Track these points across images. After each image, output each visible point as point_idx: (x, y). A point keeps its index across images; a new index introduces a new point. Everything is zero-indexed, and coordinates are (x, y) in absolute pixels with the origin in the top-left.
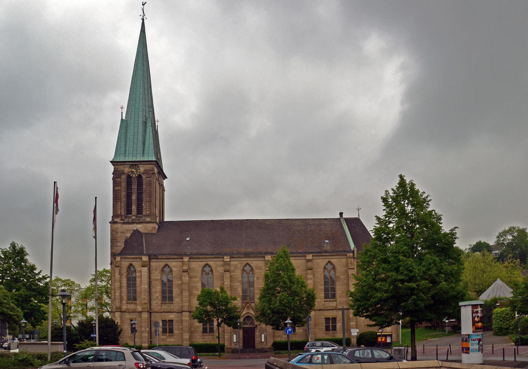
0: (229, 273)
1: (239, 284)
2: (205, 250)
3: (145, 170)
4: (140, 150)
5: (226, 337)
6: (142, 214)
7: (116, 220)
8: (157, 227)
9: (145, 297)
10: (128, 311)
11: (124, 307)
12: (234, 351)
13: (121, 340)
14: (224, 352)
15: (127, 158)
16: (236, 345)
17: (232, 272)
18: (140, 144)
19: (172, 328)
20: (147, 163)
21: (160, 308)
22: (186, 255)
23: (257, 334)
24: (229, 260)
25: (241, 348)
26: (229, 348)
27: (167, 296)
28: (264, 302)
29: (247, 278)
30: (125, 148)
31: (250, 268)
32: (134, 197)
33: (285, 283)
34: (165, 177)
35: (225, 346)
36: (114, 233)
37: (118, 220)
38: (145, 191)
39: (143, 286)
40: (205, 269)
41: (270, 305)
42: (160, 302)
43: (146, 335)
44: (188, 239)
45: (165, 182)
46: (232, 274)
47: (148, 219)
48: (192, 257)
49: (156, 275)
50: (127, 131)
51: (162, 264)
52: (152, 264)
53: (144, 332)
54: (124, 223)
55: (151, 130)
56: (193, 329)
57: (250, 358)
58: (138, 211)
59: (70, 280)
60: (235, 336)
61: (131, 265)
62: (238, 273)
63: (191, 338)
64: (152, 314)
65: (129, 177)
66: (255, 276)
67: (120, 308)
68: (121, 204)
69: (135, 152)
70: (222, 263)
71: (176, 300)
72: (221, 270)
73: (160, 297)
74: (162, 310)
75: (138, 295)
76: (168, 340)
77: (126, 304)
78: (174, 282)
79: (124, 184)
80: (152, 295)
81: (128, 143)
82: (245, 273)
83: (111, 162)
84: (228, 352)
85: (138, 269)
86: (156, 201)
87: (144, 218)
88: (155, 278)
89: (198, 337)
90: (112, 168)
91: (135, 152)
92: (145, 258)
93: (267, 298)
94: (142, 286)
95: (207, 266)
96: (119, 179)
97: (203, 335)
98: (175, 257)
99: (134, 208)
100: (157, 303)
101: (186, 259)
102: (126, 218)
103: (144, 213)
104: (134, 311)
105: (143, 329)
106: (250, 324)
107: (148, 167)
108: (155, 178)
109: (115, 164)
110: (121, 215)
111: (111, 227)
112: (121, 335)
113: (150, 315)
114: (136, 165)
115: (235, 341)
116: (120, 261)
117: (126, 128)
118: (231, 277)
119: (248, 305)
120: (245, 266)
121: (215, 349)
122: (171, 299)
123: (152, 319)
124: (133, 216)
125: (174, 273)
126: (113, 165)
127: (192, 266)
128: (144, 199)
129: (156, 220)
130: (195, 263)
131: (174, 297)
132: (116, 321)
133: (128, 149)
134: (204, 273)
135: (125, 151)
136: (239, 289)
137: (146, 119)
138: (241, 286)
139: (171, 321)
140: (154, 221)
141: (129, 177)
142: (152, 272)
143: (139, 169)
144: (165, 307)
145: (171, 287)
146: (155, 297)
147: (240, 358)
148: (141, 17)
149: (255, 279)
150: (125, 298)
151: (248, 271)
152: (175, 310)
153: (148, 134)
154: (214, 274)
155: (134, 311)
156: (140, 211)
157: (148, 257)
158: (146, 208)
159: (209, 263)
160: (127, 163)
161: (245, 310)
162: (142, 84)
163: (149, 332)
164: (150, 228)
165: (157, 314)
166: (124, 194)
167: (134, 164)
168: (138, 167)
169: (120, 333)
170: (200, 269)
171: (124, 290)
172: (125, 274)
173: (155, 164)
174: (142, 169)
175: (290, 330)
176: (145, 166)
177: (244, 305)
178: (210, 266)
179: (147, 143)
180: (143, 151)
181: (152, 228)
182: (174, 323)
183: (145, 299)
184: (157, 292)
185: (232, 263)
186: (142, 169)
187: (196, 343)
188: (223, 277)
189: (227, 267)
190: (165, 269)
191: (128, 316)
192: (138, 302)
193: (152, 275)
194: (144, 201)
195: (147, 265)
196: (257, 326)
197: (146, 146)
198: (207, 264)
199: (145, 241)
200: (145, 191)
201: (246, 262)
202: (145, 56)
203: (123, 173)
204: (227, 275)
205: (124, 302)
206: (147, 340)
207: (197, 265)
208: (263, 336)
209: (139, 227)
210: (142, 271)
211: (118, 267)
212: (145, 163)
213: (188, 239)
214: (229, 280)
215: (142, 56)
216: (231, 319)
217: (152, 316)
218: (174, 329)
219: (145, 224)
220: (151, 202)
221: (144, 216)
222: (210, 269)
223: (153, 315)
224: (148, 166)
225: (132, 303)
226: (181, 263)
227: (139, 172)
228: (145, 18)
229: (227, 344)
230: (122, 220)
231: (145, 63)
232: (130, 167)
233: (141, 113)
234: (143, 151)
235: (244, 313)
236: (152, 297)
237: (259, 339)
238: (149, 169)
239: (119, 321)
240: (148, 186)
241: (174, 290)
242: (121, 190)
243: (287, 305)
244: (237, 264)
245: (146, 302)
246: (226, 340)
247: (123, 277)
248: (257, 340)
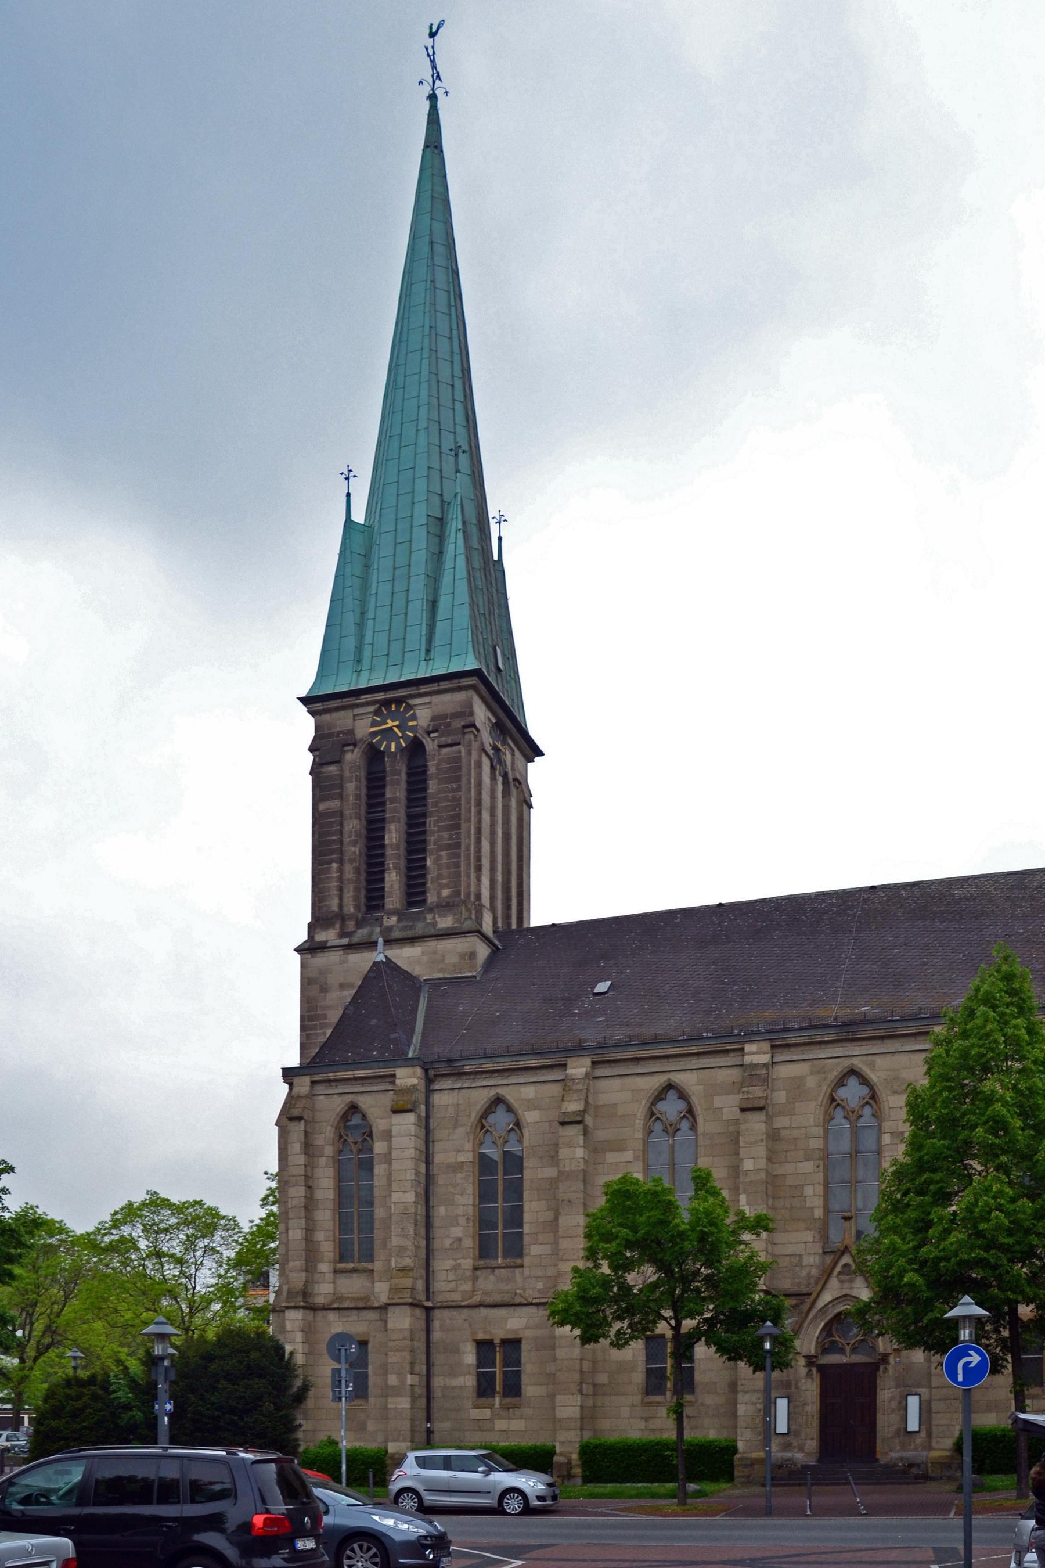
0: (760, 1116)
1: (809, 1166)
2: (669, 1024)
3: (434, 719)
4: (416, 636)
5: (741, 1409)
6: (424, 901)
7: (321, 937)
8: (483, 951)
9: (402, 1242)
10: (337, 1306)
11: (324, 1291)
12: (787, 1475)
13: (306, 1425)
14: (731, 1478)
15: (365, 675)
16: (787, 1447)
17: (782, 1113)
18: (418, 611)
19: (518, 1374)
20: (444, 685)
21: (467, 1287)
22: (578, 1049)
23: (886, 1394)
24: (765, 1058)
25: (812, 1461)
26: (752, 1463)
27: (499, 1237)
28: (894, 1229)
29: (847, 1135)
30: (361, 637)
31: (864, 1091)
32: (394, 835)
33: (998, 1125)
34: (534, 751)
35: (734, 1450)
36: (314, 990)
37: (328, 935)
38: (435, 804)
39: (395, 1197)
40: (661, 1106)
41: (923, 1243)
42: (467, 1263)
43: (404, 1403)
44: (602, 987)
45: (536, 773)
46: (780, 1122)
47: (446, 922)
48: (604, 1057)
49: (456, 1149)
50: (367, 567)
51: (481, 1097)
52: (437, 1099)
53: (396, 1392)
54: (350, 947)
55: (461, 549)
56: (602, 1378)
57: (819, 1512)
58: (409, 895)
59: (199, 1203)
60: (782, 1405)
61: (353, 1108)
62: (807, 1118)
63: (588, 1417)
64: (437, 1313)
65: (374, 756)
66: (887, 1125)
67: (305, 1294)
68: (340, 870)
69: (396, 646)
70: (735, 1074)
71: (535, 1250)
72: (728, 1104)
73: (469, 1243)
74: (477, 1299)
75: (378, 1234)
76: (500, 1425)
77: (329, 1276)
78: (528, 1175)
79: (353, 788)
80: (437, 1233)
81: (370, 615)
82: (839, 1113)
83: (305, 701)
84: (748, 1481)
85: (379, 1124)
86: (478, 841)
87: (429, 916)
88: (452, 1158)
89: (625, 1411)
90: (306, 726)
91: (396, 646)
92: (408, 1077)
93: (911, 1214)
94: (397, 1193)
95: (672, 1095)
96: (332, 768)
97: (644, 1404)
98: (533, 1062)
99: (393, 880)
100: (456, 1268)
101: (578, 1068)
102: (359, 925)
103: (431, 898)
104: (363, 1306)
105: (393, 1380)
106: (854, 1350)
107: (448, 702)
108: (475, 745)
109: (318, 706)
110: (342, 917)
111: (303, 966)
112: (310, 1403)
113: (428, 1321)
114: (399, 701)
115: (782, 1427)
116: (312, 1095)
117: (367, 556)
118: (773, 1136)
119: (846, 1259)
120: (841, 1082)
121: (696, 1467)
122: (515, 1248)
123: (437, 1335)
124: (391, 913)
125: (526, 1132)
126: (312, 713)
127: (604, 1099)
128: (432, 839)
129: (479, 919)
130: (616, 1083)
131: (526, 1239)
132: (288, 1348)
133: (368, 639)
134: (658, 1127)
135: (359, 648)
136: (809, 1191)
137: (444, 504)
138: (820, 1177)
139: (513, 1344)
140: (468, 925)
141: (374, 756)
142: (438, 1134)
143: (414, 718)
144: (490, 1284)
145: (515, 1190)
146: (447, 1242)
147: (768, 1512)
148: (426, 90)
149: (886, 1139)
150: (327, 1248)
151: (854, 1103)
152: (531, 1295)
153: (448, 564)
154: (701, 1129)
155: (363, 1306)
156: (415, 892)
157: (419, 1071)
158: (439, 876)
159: (678, 1078)
160: (365, 698)
161: (834, 1282)
162: (425, 362)
163: (421, 1391)
164: (452, 959)
165: (454, 1313)
166: (353, 825)
167: (393, 698)
168: (410, 707)
169: (300, 1397)
170: (640, 1110)
171: (325, 1216)
172: (329, 1150)
173: (473, 687)
174: (423, 714)
175: (975, 1359)
176: (435, 699)
177: (829, 1259)
178: (682, 1095)
179: (444, 602)
180: (430, 640)
181: (462, 956)
182: (527, 1354)
183: (402, 1249)
184: (454, 1221)
185: (784, 1072)
186: (423, 714)
187: (612, 1438)
188: (734, 1139)
189: (757, 1091)
190: (491, 1119)
191: (336, 1324)
192: (378, 1265)
193: (438, 1147)
194: (431, 847)
195: (416, 1105)
196: (884, 1359)
197: (442, 612)
198: (670, 1086)
199: (429, 1008)
200: (435, 804)
201: (846, 1063)
202: (440, 249)
203: (349, 741)
204: (757, 1124)
205: (324, 1267)
206: (407, 1425)
207: (626, 1092)
208: (913, 1402)
209: (406, 956)
210: (395, 1130)
211: (299, 1118)
212: (434, 687)
213: (602, 987)
214: (761, 1151)
215: (426, 249)
216: (745, 1328)
217: (436, 1324)
218: (524, 1379)
219: (432, 944)
220: (458, 845)
221: (431, 910)
222: (682, 1105)
223: (440, 1318)
224: (446, 697)
225: (354, 1270)
226: (556, 1089)
227: (413, 729)
228: (439, 93)
229: (746, 1444)
230: (343, 934)
231: (441, 277)
232: (377, 713)
233: (421, 485)
234: (430, 640)
235: (827, 1297)
236: (436, 1244)
237: (894, 1419)
238: (450, 709)
239: (300, 1348)
240: (449, 780)
241: (527, 1207)
242: (341, 813)
243: (1004, 1240)
244: (803, 1073)
245: (408, 1262)
246: (741, 1422)
247: (323, 1161)
248: (885, 1423)
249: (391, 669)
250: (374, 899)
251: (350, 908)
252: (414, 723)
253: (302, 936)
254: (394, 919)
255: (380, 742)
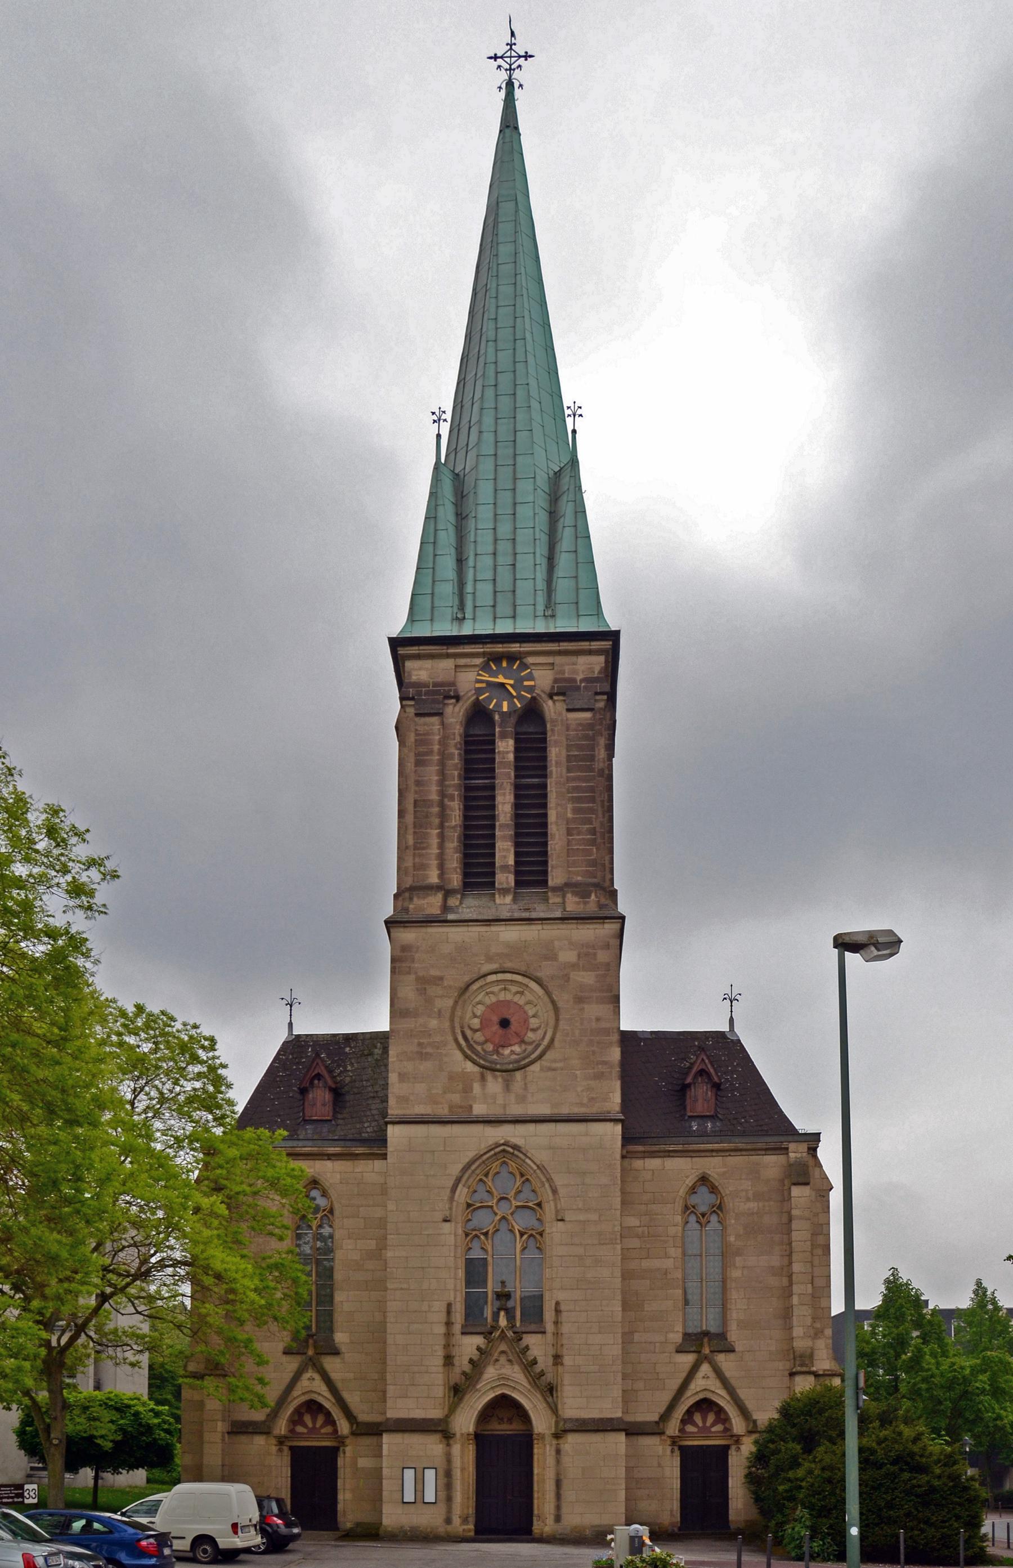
99: (505, 852)
114: (512, 658)
141: (479, 715)
156: (532, 873)
167: (502, 650)
176: (558, 660)
186: (542, 679)
203: (450, 693)
227: (530, 689)
249: (581, 619)
250: (478, 874)
251: (455, 880)
252: (532, 683)
253: (388, 910)
254: (508, 899)
255: (489, 699)
